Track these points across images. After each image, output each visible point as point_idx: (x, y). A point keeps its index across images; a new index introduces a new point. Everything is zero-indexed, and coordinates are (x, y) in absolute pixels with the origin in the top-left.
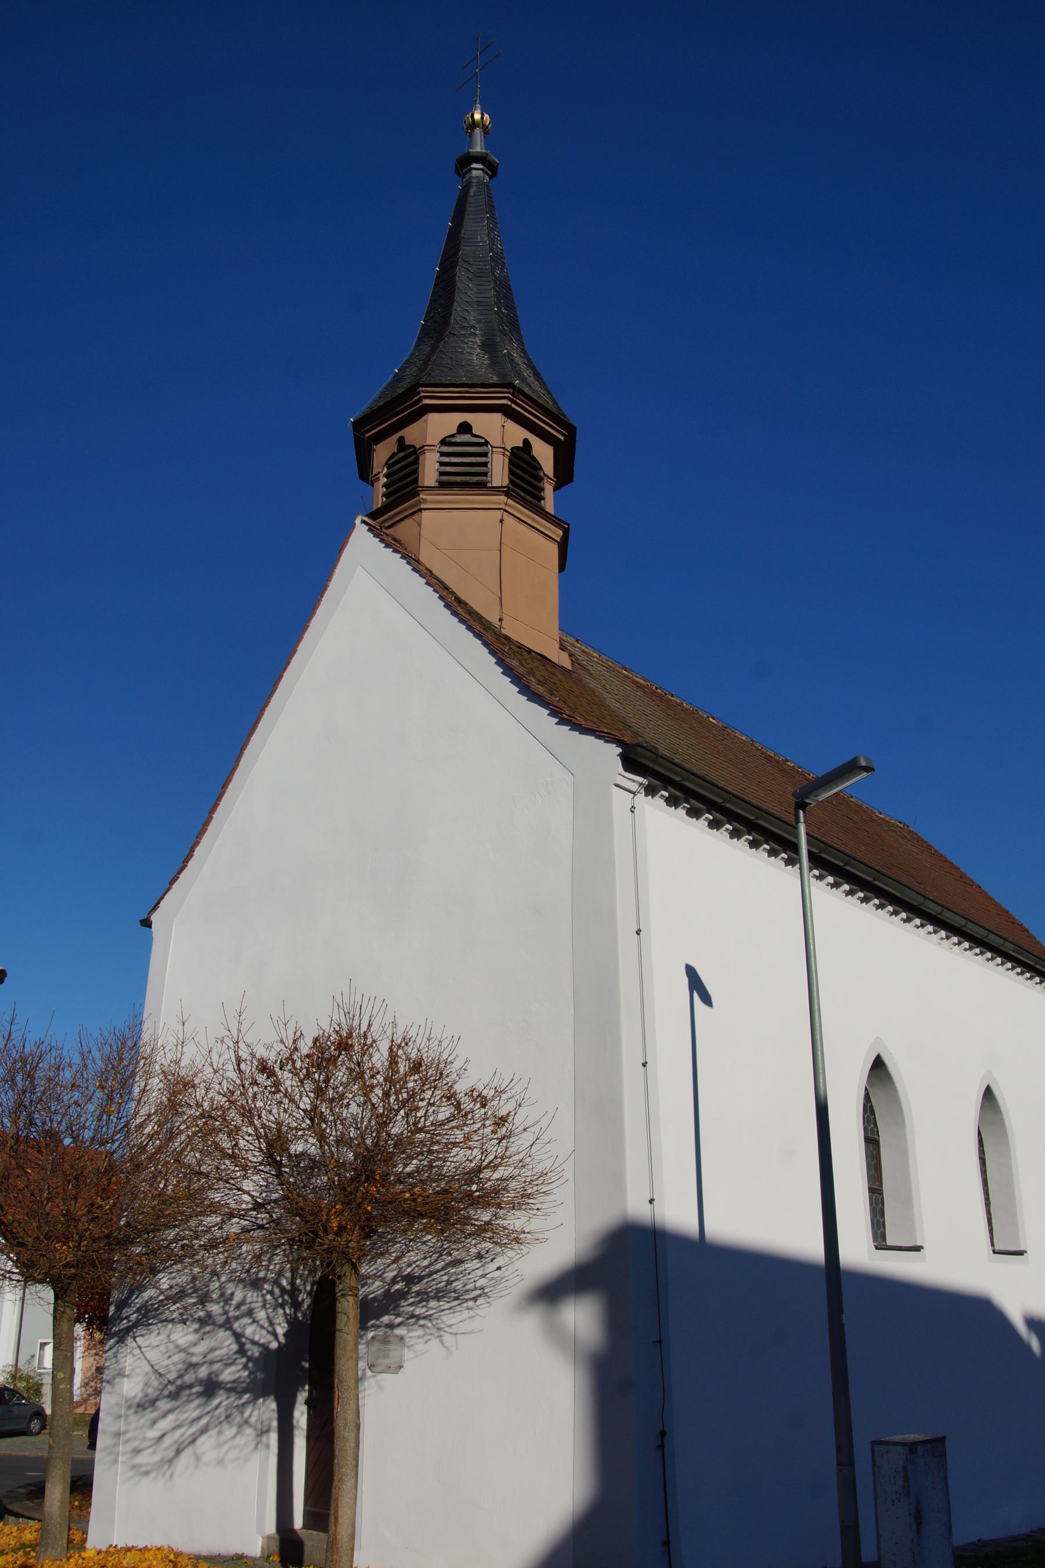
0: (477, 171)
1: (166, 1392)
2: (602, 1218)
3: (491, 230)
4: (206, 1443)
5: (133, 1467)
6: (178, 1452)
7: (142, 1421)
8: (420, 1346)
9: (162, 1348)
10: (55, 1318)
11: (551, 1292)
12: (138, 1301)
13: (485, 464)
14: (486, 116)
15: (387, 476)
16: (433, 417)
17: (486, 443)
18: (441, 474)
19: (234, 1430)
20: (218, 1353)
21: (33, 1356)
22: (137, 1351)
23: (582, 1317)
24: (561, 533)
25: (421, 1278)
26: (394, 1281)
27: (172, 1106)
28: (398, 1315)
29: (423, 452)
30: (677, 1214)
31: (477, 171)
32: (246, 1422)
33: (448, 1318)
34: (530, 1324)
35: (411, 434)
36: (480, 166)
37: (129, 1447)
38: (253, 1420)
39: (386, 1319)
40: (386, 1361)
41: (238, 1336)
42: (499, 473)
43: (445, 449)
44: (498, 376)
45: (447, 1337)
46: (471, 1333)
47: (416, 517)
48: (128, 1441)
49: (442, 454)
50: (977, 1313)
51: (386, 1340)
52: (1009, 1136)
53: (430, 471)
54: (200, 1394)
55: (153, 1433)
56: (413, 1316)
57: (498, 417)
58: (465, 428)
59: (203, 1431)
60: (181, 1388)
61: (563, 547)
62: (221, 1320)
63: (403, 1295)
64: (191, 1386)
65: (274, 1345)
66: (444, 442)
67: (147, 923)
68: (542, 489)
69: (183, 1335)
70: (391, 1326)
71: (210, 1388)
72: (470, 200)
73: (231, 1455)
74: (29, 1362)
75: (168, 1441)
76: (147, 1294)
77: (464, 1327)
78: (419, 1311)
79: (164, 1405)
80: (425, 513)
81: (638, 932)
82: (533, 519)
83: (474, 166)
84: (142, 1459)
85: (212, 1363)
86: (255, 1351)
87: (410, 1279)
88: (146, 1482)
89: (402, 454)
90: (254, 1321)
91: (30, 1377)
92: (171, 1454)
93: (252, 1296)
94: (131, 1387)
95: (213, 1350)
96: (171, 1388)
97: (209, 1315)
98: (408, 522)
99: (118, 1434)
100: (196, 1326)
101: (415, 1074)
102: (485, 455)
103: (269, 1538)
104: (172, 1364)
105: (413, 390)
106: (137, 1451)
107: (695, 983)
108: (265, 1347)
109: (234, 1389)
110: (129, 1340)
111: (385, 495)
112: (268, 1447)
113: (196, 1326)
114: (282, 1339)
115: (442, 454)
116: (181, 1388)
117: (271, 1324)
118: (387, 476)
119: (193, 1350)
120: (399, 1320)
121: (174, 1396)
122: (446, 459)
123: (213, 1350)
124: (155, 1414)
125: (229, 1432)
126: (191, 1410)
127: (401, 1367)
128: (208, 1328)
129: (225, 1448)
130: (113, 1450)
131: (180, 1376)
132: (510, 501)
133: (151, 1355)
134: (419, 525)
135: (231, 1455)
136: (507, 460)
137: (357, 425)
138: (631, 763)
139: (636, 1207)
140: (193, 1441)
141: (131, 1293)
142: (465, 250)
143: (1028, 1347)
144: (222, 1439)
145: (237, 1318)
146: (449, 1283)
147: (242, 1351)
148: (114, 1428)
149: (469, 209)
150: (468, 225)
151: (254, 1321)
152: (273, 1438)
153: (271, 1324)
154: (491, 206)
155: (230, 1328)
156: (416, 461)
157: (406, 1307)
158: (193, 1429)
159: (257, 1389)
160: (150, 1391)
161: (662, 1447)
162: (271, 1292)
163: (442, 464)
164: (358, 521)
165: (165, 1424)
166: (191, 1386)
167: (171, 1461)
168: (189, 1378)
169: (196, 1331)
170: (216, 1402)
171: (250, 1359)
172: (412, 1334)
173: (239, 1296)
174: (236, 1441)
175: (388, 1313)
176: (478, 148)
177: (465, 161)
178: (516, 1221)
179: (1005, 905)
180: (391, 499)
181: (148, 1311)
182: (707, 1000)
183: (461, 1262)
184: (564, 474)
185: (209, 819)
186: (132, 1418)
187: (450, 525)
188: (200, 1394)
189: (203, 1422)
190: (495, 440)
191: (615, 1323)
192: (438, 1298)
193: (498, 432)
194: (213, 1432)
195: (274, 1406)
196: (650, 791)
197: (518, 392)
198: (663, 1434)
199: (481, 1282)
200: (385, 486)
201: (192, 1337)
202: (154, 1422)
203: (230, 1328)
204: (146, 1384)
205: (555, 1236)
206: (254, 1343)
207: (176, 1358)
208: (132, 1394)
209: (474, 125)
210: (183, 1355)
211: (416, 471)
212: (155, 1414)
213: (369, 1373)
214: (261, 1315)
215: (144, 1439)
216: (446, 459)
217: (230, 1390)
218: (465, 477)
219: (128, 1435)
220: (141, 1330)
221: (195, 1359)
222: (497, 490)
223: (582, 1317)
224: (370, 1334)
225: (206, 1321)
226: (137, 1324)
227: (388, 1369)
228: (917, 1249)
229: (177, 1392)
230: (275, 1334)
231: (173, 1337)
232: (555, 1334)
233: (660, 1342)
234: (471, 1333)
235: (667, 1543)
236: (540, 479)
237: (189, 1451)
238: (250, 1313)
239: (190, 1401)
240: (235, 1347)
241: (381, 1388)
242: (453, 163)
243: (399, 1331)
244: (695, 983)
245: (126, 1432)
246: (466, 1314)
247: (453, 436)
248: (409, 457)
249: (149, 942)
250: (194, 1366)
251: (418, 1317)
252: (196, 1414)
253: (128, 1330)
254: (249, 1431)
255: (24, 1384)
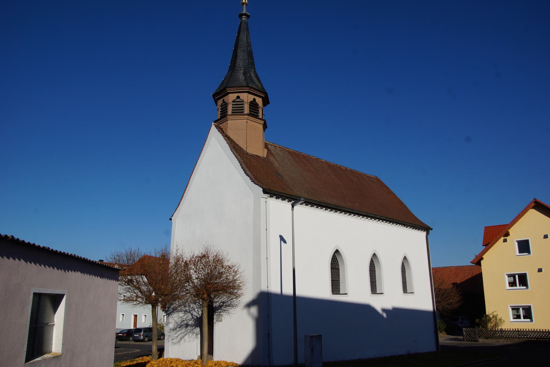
0: (244, 18)
2: (257, 291)
3: (247, 36)
4: (186, 337)
8: (226, 316)
11: (249, 305)
12: (172, 307)
16: (230, 95)
23: (254, 310)
27: (176, 263)
30: (275, 289)
31: (244, 18)
33: (230, 311)
34: (245, 311)
35: (225, 98)
41: (192, 314)
42: (247, 110)
50: (367, 309)
51: (219, 315)
53: (230, 111)
57: (246, 94)
58: (238, 97)
59: (186, 335)
60: (181, 326)
63: (222, 306)
66: (233, 101)
67: (171, 219)
69: (181, 314)
70: (220, 312)
71: (187, 325)
75: (179, 337)
76: (175, 305)
77: (233, 312)
79: (178, 329)
86: (195, 318)
87: (223, 303)
94: (171, 326)
101: (218, 261)
104: (179, 321)
105: (225, 89)
106: (173, 339)
107: (282, 239)
108: (197, 317)
109: (191, 326)
116: (181, 326)
121: (180, 327)
125: (191, 335)
126: (183, 330)
130: (168, 339)
137: (213, 96)
138: (265, 192)
139: (264, 288)
142: (240, 43)
143: (382, 316)
147: (193, 318)
149: (242, 31)
150: (241, 35)
152: (199, 336)
157: (223, 308)
159: (196, 325)
165: (179, 333)
168: (183, 323)
172: (224, 314)
173: (192, 306)
177: (241, 16)
178: (239, 292)
179: (401, 199)
184: (266, 102)
185: (183, 195)
191: (260, 311)
193: (247, 98)
196: (271, 197)
197: (251, 88)
198: (269, 334)
205: (248, 294)
214: (196, 310)
218: (238, 111)
222: (245, 115)
223: (254, 310)
225: (186, 311)
227: (220, 321)
228: (346, 294)
232: (249, 313)
235: (269, 355)
236: (258, 108)
238: (194, 309)
248: (225, 106)
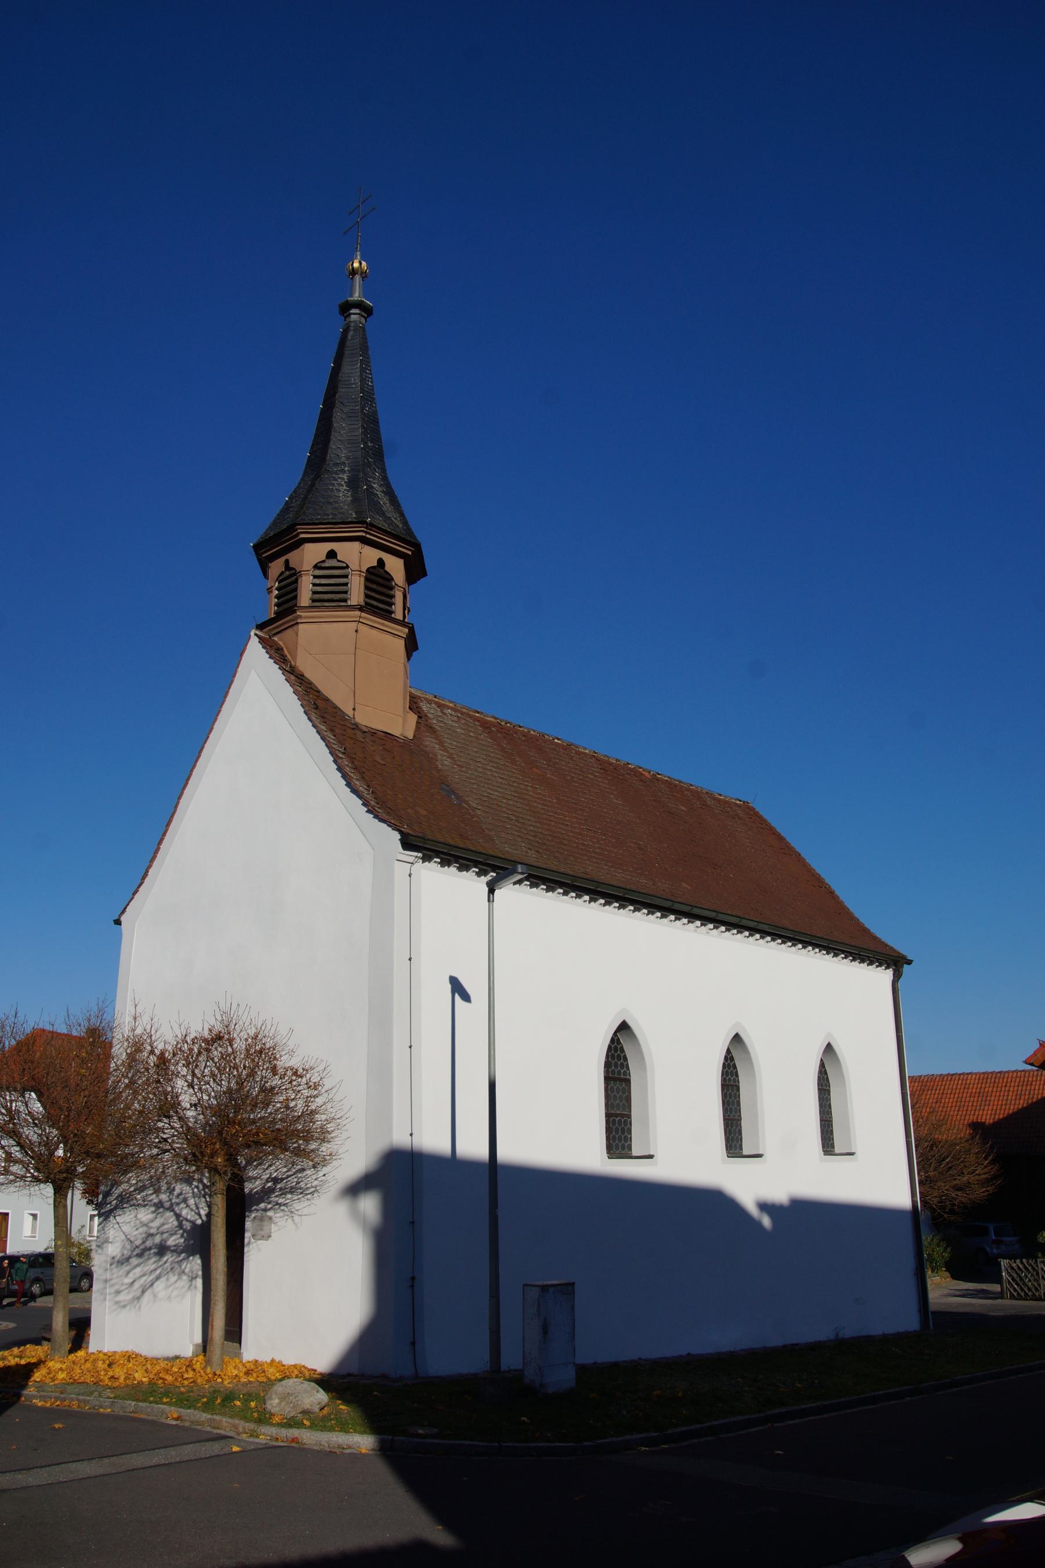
0: (355, 315)
1: (135, 1253)
4: (159, 1285)
5: (117, 1303)
6: (143, 1292)
7: (121, 1273)
9: (132, 1224)
10: (55, 1206)
11: (354, 1189)
12: (117, 1192)
13: (346, 584)
14: (364, 263)
15: (278, 589)
16: (308, 546)
17: (347, 567)
18: (314, 593)
19: (176, 1278)
20: (166, 1227)
21: (83, 1226)
22: (116, 1226)
23: (370, 1205)
24: (407, 630)
25: (282, 1179)
26: (267, 1181)
28: (269, 1203)
29: (301, 576)
31: (355, 315)
32: (183, 1272)
33: (297, 1206)
34: (342, 1209)
35: (293, 557)
36: (357, 311)
37: (113, 1290)
38: (187, 1271)
39: (262, 1205)
40: (262, 1233)
41: (178, 1216)
42: (356, 594)
43: (318, 572)
44: (356, 513)
45: (296, 1218)
46: (309, 1215)
47: (295, 628)
48: (112, 1285)
49: (315, 577)
50: (713, 1203)
51: (262, 1219)
52: (843, 1064)
54: (156, 1254)
55: (128, 1280)
56: (277, 1204)
57: (356, 545)
58: (332, 554)
59: (158, 1278)
61: (411, 645)
62: (167, 1205)
63: (272, 1190)
64: (150, 1249)
65: (199, 1222)
66: (316, 567)
67: (118, 922)
68: (393, 596)
69: (145, 1215)
70: (265, 1210)
71: (162, 1250)
72: (348, 343)
73: (175, 1293)
74: (80, 1231)
75: (137, 1285)
76: (124, 1186)
77: (305, 1211)
78: (281, 1201)
79: (134, 1261)
80: (301, 626)
81: (410, 959)
82: (383, 624)
83: (353, 311)
84: (122, 1297)
85: (162, 1233)
86: (187, 1226)
87: (276, 1181)
88: (124, 1311)
89: (287, 573)
90: (187, 1206)
91: (81, 1244)
92: (139, 1293)
93: (186, 1188)
94: (114, 1249)
95: (163, 1224)
96: (137, 1251)
97: (161, 1202)
98: (289, 632)
99: (106, 1281)
100: (153, 1209)
101: (261, 1053)
102: (346, 576)
103: (197, 1345)
104: (137, 1235)
105: (292, 528)
106: (118, 1292)
107: (457, 988)
108: (193, 1223)
109: (176, 1250)
110: (112, 1218)
111: (277, 605)
112: (196, 1287)
113: (153, 1209)
114: (204, 1218)
115: (315, 577)
117: (197, 1208)
118: (278, 589)
119: (151, 1225)
120: (269, 1206)
121: (140, 1255)
122: (317, 581)
123: (163, 1224)
124: (128, 1268)
125: (173, 1278)
126: (151, 1264)
127: (270, 1236)
128: (161, 1210)
129: (171, 1289)
130: (103, 1292)
131: (144, 1242)
132: (363, 615)
133: (125, 1228)
134: (297, 635)
135: (175, 1293)
136: (363, 579)
137: (257, 548)
138: (407, 844)
139: (400, 1138)
140: (152, 1285)
141: (112, 1186)
142: (342, 391)
143: (758, 1224)
144: (169, 1283)
145: (178, 1204)
146: (298, 1183)
147: (180, 1226)
148: (103, 1277)
149: (347, 353)
151: (187, 1206)
152: (199, 1282)
153: (197, 1208)
154: (364, 348)
155: (173, 1210)
156: (296, 581)
158: (151, 1277)
159: (189, 1250)
160: (125, 1252)
161: (412, 1286)
162: (197, 1187)
163: (314, 585)
164: (252, 633)
166: (150, 1249)
167: (138, 1298)
168: (148, 1243)
169: (153, 1212)
170: (165, 1259)
171: (185, 1231)
174: (177, 1284)
175: (263, 1201)
176: (356, 296)
177: (345, 308)
178: (325, 1149)
180: (281, 609)
181: (123, 1199)
182: (466, 997)
183: (303, 1170)
186: (115, 1270)
187: (320, 637)
188: (156, 1254)
189: (158, 1272)
190: (354, 565)
191: (388, 1209)
192: (292, 1193)
193: (358, 557)
194: (163, 1279)
195: (199, 1261)
196: (426, 858)
198: (413, 1278)
199: (316, 1183)
200: (277, 597)
201: (151, 1216)
202: (128, 1273)
203: (173, 1210)
204: (123, 1247)
205: (352, 1155)
206: (187, 1220)
207: (141, 1230)
208: (114, 1254)
209: (354, 272)
210: (145, 1229)
211: (296, 590)
212: (128, 1268)
213: (252, 1240)
214: (191, 1202)
215: (122, 1284)
216: (317, 581)
217: (172, 1251)
218: (332, 597)
219: (112, 1282)
220: (119, 1212)
221: (152, 1231)
222: (352, 608)
223: (370, 1205)
224: (253, 1215)
225: (159, 1205)
226: (116, 1208)
227: (263, 1238)
229: (142, 1253)
230: (199, 1215)
231: (139, 1216)
232: (355, 1215)
233: (413, 1222)
234: (309, 1215)
236: (392, 588)
237: (149, 1291)
238: (185, 1200)
239: (149, 1259)
240: (176, 1223)
241: (259, 1250)
242: (337, 310)
243: (270, 1213)
244: (457, 988)
245: (111, 1280)
246: (306, 1203)
247: (323, 561)
249: (120, 934)
250: (152, 1235)
251: (280, 1205)
252: (153, 1267)
253: (111, 1211)
254: (185, 1277)
255: (75, 1250)
